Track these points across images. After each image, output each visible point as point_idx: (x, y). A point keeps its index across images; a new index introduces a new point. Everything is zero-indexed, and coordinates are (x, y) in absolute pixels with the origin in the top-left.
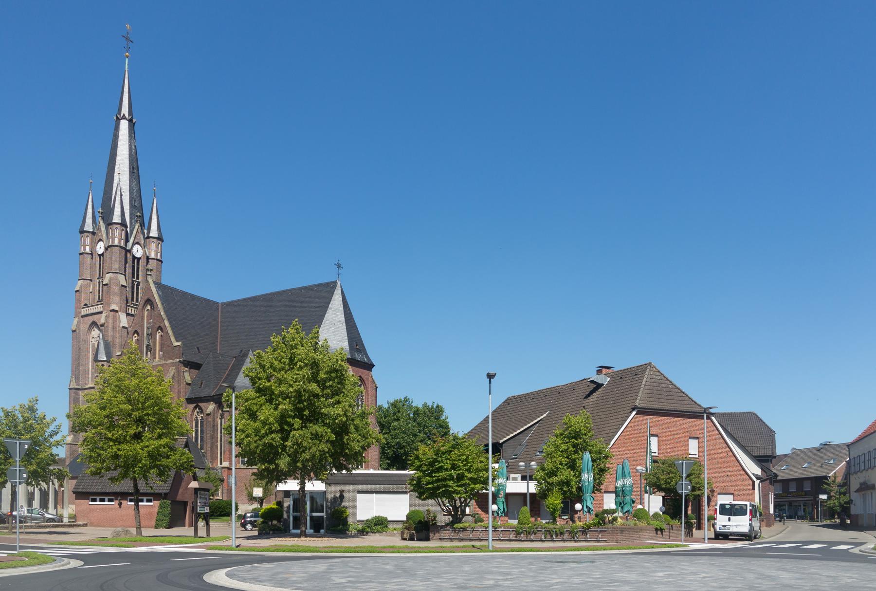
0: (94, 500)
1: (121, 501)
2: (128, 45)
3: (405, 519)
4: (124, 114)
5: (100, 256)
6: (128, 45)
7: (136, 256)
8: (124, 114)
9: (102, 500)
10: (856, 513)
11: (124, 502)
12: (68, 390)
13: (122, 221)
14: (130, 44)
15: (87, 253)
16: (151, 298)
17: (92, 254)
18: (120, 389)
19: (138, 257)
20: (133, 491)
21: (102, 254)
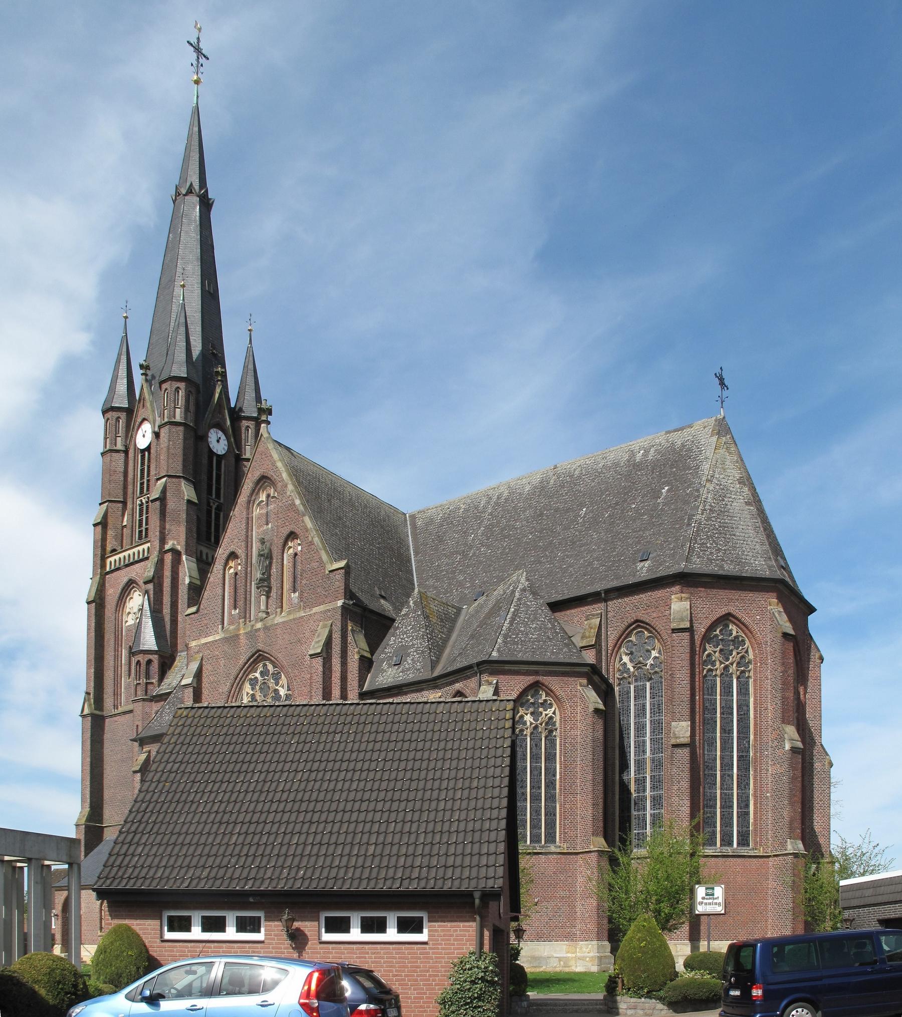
0: (341, 925)
1: (296, 924)
2: (198, 62)
3: (602, 998)
4: (191, 185)
5: (143, 451)
6: (198, 62)
7: (215, 451)
8: (191, 185)
9: (374, 925)
10: (607, 980)
11: (307, 927)
12: (80, 718)
13: (188, 374)
14: (202, 60)
15: (118, 451)
16: (270, 474)
17: (126, 452)
18: (271, 544)
19: (219, 453)
20: (723, 912)
21: (148, 448)
